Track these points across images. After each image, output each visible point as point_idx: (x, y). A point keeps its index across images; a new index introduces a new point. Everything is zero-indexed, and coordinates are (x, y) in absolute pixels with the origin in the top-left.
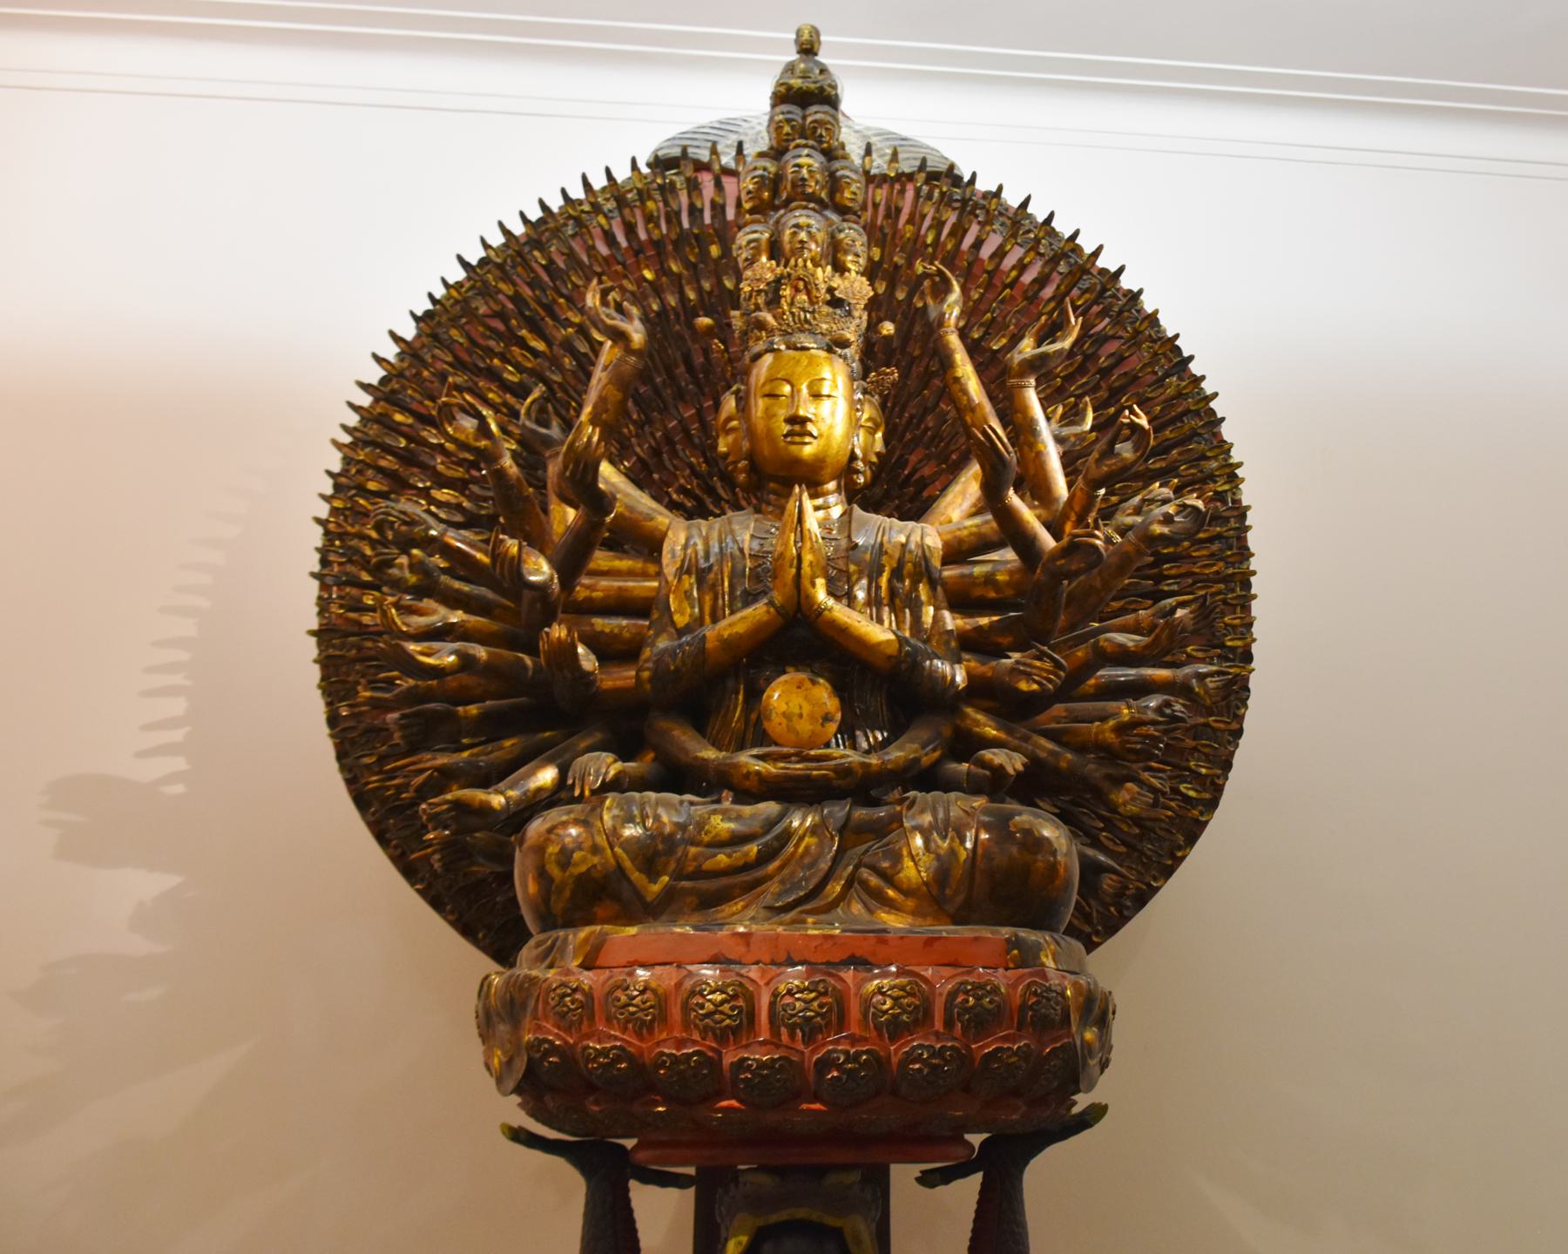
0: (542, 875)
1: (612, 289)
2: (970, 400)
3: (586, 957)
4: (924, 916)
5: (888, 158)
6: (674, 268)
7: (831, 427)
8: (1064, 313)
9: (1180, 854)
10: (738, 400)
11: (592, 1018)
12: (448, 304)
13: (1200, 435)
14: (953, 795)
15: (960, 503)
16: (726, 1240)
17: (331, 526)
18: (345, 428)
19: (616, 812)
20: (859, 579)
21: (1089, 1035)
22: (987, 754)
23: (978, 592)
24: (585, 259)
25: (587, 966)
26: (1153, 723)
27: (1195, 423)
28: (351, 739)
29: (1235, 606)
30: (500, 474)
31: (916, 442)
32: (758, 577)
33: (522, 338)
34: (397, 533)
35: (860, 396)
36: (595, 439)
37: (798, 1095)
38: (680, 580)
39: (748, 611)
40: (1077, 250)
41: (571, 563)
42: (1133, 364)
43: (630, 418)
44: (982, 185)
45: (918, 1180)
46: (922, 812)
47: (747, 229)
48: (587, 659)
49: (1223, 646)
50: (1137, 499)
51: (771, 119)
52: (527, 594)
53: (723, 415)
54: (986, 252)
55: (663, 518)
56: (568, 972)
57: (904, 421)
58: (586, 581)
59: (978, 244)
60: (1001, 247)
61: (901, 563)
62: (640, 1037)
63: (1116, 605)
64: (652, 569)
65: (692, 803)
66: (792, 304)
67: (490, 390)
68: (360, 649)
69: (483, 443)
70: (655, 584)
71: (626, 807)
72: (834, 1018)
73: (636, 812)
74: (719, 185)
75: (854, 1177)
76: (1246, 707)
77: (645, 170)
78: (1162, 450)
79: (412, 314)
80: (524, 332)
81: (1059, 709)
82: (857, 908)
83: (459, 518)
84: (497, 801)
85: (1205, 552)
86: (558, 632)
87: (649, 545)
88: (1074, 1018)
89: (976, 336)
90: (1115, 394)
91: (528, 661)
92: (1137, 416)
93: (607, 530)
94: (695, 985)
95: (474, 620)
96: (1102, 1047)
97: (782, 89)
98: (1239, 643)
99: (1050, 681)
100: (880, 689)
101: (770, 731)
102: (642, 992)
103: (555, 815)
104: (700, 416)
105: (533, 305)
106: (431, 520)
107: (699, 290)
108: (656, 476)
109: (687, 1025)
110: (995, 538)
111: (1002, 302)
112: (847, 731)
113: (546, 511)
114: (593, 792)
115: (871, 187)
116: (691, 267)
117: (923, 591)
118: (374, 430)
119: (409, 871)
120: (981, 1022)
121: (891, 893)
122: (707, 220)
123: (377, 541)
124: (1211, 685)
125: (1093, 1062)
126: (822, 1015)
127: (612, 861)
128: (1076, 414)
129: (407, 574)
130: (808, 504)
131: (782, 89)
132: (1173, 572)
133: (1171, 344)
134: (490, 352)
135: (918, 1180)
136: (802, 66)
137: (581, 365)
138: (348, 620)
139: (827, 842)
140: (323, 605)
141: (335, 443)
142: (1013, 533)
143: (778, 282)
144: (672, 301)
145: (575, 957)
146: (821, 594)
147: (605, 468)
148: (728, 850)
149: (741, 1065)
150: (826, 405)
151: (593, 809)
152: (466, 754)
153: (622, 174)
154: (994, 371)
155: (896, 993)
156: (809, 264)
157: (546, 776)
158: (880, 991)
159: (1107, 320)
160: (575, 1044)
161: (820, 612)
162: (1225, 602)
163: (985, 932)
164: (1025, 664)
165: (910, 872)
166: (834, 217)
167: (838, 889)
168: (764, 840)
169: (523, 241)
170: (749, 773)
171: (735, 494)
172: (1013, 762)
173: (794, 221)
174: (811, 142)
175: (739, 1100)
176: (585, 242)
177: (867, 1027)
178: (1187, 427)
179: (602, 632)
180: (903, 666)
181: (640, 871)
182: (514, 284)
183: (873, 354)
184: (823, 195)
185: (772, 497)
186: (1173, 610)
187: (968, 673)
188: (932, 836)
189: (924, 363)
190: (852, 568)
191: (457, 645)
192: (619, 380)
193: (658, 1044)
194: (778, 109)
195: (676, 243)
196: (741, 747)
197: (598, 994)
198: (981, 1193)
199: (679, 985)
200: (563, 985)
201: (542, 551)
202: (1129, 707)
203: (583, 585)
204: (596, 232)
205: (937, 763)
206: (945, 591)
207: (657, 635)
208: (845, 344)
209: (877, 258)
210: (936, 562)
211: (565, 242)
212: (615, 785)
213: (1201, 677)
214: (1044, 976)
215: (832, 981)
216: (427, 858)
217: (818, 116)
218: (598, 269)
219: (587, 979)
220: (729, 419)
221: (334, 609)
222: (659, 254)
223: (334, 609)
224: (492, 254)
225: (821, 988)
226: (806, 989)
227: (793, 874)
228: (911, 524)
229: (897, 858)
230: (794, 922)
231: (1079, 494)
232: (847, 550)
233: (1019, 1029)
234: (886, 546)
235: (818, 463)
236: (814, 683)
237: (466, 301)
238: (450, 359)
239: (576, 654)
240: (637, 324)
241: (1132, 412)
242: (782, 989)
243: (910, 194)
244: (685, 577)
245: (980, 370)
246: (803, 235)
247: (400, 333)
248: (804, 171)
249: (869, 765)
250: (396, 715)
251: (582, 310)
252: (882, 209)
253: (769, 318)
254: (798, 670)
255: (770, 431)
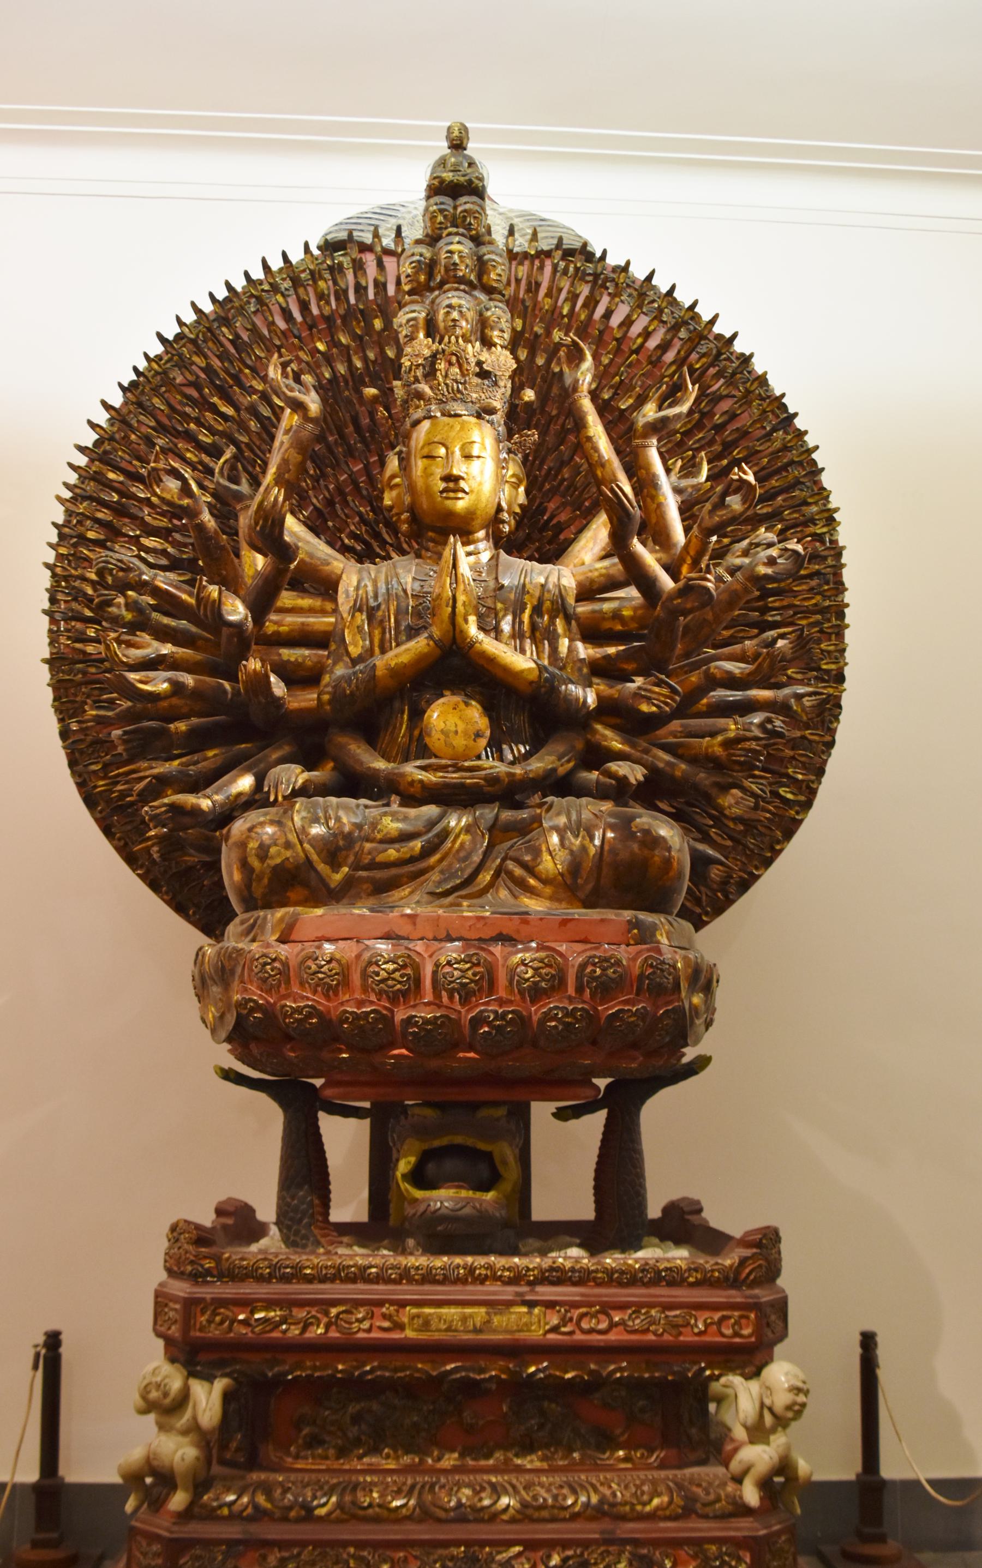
0: (244, 865)
1: (291, 361)
2: (600, 456)
3: (282, 933)
4: (559, 901)
5: (529, 237)
6: (343, 340)
7: (480, 484)
8: (682, 376)
9: (778, 847)
10: (401, 460)
11: (288, 982)
12: (149, 375)
13: (803, 483)
14: (584, 800)
15: (591, 547)
16: (398, 1160)
17: (58, 570)
18: (66, 485)
19: (304, 814)
20: (504, 616)
21: (697, 999)
22: (613, 766)
23: (607, 625)
24: (266, 333)
25: (283, 940)
26: (756, 739)
27: (797, 472)
28: (83, 752)
29: (830, 634)
30: (201, 528)
31: (554, 491)
32: (420, 614)
33: (214, 405)
34: (115, 578)
35: (505, 455)
36: (281, 499)
37: (456, 1045)
38: (353, 616)
39: (411, 644)
40: (696, 317)
41: (261, 603)
42: (744, 420)
43: (307, 472)
44: (611, 261)
45: (554, 1115)
46: (558, 814)
47: (407, 309)
48: (278, 687)
49: (819, 669)
50: (745, 543)
51: (426, 209)
52: (225, 631)
53: (388, 473)
54: (615, 321)
55: (338, 563)
56: (268, 946)
57: (543, 472)
58: (273, 617)
59: (608, 314)
60: (628, 317)
61: (541, 601)
62: (328, 998)
63: (726, 633)
64: (329, 606)
65: (366, 807)
66: (446, 376)
67: (188, 450)
68: (85, 673)
69: (186, 502)
70: (332, 620)
71: (312, 809)
72: (485, 984)
73: (321, 815)
74: (380, 265)
75: (501, 1112)
76: (838, 721)
77: (316, 252)
78: (768, 497)
79: (120, 385)
80: (215, 400)
81: (676, 725)
82: (504, 893)
83: (164, 562)
84: (205, 804)
85: (804, 587)
86: (254, 664)
87: (327, 587)
88: (684, 985)
89: (606, 397)
90: (728, 447)
91: (227, 686)
92: (745, 473)
93: (290, 574)
94: (372, 956)
95: (181, 652)
96: (707, 1010)
97: (436, 182)
98: (833, 667)
99: (666, 704)
100: (524, 709)
101: (430, 745)
102: (329, 962)
103: (254, 816)
104: (367, 469)
105: (222, 375)
106: (143, 567)
107: (365, 359)
108: (330, 524)
109: (365, 989)
110: (622, 579)
111: (629, 366)
112: (495, 745)
113: (238, 556)
114: (285, 797)
115: (514, 263)
116: (355, 337)
117: (560, 625)
118: (90, 487)
119: (131, 860)
120: (605, 990)
121: (532, 881)
122: (371, 296)
123: (98, 583)
124: (808, 704)
125: (699, 1022)
126: (476, 982)
127: (302, 854)
128: (694, 466)
129: (124, 612)
130: (461, 551)
131: (436, 182)
132: (777, 604)
133: (778, 403)
134: (187, 418)
135: (554, 1115)
136: (453, 160)
137: (263, 427)
138: (74, 649)
139: (479, 838)
140: (54, 636)
141: (58, 498)
142: (634, 573)
143: (434, 356)
144: (342, 369)
145: (273, 933)
146: (472, 629)
147: (290, 521)
148: (397, 846)
149: (409, 1021)
150: (476, 464)
151: (285, 812)
152: (176, 763)
153: (296, 256)
154: (622, 427)
155: (536, 964)
156: (460, 340)
157: (245, 783)
158: (523, 963)
159: (722, 381)
160: (275, 1003)
161: (472, 645)
162: (821, 631)
163: (610, 914)
164: (645, 690)
165: (548, 865)
166: (482, 297)
167: (488, 878)
168: (425, 838)
169: (211, 318)
170: (413, 781)
171: (397, 538)
172: (634, 773)
173: (447, 302)
174: (461, 230)
175: (407, 1049)
176: (266, 319)
177: (512, 992)
178: (790, 477)
179: (288, 661)
180: (543, 690)
181: (325, 863)
182: (206, 357)
183: (517, 417)
184: (472, 277)
185: (431, 545)
186: (774, 641)
187: (598, 695)
188: (568, 833)
189: (560, 421)
190: (499, 606)
191: (169, 674)
192: (301, 446)
193: (342, 1004)
194: (432, 201)
195: (344, 318)
196: (406, 759)
197: (293, 963)
198: (606, 1126)
199: (358, 956)
200: (264, 955)
201: (236, 593)
202: (736, 723)
203: (271, 621)
204: (275, 309)
205: (571, 773)
206: (579, 625)
207: (335, 664)
208: (492, 411)
209: (519, 329)
210: (571, 600)
211: (248, 318)
212: (302, 792)
213: (799, 697)
214: (659, 951)
215: (483, 954)
216: (148, 849)
217: (468, 206)
218: (278, 343)
219: (284, 951)
220: (393, 476)
221: (63, 640)
222: (329, 328)
223: (63, 640)
224: (186, 330)
225: (474, 960)
226: (462, 961)
227: (450, 865)
228: (549, 567)
229: (537, 853)
230: (452, 905)
231: (694, 540)
232: (495, 590)
233: (637, 994)
234: (528, 586)
235: (470, 515)
236: (467, 704)
237: (165, 372)
238: (153, 424)
239: (269, 682)
240: (313, 394)
241: (741, 469)
242: (443, 960)
243: (548, 269)
244: (358, 614)
245: (609, 428)
246: (455, 315)
247: (111, 402)
248: (456, 257)
249: (513, 775)
250: (119, 732)
251: (264, 379)
252: (523, 283)
253: (425, 388)
254: (453, 694)
255: (428, 490)
